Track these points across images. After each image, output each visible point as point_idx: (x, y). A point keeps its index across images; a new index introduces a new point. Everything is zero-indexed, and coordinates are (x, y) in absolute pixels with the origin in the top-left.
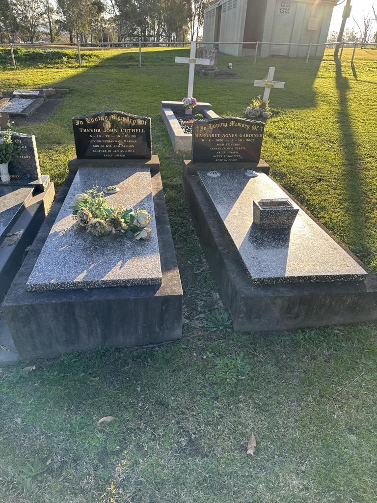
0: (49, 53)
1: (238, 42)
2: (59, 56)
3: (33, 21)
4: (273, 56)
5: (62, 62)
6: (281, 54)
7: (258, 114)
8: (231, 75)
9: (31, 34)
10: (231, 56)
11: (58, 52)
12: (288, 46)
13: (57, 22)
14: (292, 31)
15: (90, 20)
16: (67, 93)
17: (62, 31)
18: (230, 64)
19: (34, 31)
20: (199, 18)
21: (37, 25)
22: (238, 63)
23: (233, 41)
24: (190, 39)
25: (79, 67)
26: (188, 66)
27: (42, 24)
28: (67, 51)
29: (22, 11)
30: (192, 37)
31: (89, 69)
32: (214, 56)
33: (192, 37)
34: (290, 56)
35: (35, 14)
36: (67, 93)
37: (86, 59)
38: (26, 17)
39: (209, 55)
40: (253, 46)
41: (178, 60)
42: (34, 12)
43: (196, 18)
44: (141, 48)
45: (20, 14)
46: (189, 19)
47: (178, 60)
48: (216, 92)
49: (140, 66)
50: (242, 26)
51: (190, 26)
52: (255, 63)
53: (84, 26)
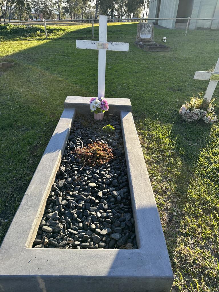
0: (29, 28)
1: (173, 18)
2: (35, 30)
3: (50, 8)
4: (199, 29)
5: (35, 35)
6: (205, 27)
7: (197, 118)
8: (163, 47)
9: (49, 15)
10: (168, 28)
11: (35, 28)
12: (211, 21)
13: (63, 8)
14: (215, 9)
15: (82, 6)
16: (12, 66)
17: (66, 13)
18: (165, 38)
19: (51, 13)
20: (148, 4)
21: (52, 10)
22: (172, 35)
23: (168, 19)
24: (142, 17)
25: (46, 39)
26: (96, 52)
27: (55, 9)
28: (42, 27)
29: (44, 2)
30: (143, 15)
31: (52, 41)
32: (151, 30)
33: (143, 15)
34: (211, 29)
35: (51, 3)
36: (12, 66)
37: (54, 33)
38: (46, 5)
39: (147, 29)
40: (185, 21)
41: (81, 44)
42: (51, 2)
43: (146, 3)
44: (94, 24)
45: (43, 4)
46: (141, 4)
47: (81, 44)
48: (148, 68)
49: (93, 38)
50: (176, 6)
51: (142, 9)
52: (186, 35)
53: (78, 10)
